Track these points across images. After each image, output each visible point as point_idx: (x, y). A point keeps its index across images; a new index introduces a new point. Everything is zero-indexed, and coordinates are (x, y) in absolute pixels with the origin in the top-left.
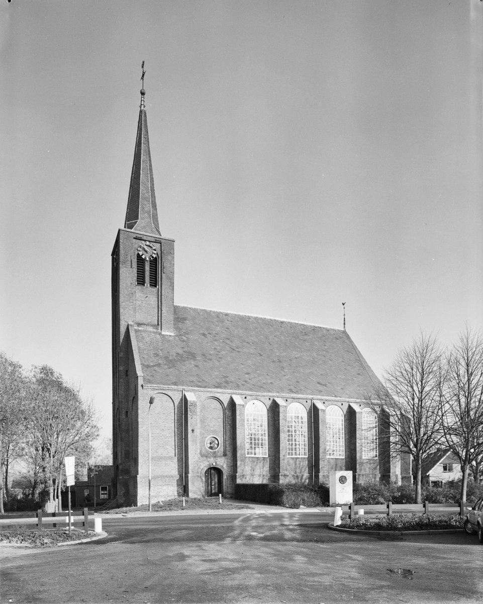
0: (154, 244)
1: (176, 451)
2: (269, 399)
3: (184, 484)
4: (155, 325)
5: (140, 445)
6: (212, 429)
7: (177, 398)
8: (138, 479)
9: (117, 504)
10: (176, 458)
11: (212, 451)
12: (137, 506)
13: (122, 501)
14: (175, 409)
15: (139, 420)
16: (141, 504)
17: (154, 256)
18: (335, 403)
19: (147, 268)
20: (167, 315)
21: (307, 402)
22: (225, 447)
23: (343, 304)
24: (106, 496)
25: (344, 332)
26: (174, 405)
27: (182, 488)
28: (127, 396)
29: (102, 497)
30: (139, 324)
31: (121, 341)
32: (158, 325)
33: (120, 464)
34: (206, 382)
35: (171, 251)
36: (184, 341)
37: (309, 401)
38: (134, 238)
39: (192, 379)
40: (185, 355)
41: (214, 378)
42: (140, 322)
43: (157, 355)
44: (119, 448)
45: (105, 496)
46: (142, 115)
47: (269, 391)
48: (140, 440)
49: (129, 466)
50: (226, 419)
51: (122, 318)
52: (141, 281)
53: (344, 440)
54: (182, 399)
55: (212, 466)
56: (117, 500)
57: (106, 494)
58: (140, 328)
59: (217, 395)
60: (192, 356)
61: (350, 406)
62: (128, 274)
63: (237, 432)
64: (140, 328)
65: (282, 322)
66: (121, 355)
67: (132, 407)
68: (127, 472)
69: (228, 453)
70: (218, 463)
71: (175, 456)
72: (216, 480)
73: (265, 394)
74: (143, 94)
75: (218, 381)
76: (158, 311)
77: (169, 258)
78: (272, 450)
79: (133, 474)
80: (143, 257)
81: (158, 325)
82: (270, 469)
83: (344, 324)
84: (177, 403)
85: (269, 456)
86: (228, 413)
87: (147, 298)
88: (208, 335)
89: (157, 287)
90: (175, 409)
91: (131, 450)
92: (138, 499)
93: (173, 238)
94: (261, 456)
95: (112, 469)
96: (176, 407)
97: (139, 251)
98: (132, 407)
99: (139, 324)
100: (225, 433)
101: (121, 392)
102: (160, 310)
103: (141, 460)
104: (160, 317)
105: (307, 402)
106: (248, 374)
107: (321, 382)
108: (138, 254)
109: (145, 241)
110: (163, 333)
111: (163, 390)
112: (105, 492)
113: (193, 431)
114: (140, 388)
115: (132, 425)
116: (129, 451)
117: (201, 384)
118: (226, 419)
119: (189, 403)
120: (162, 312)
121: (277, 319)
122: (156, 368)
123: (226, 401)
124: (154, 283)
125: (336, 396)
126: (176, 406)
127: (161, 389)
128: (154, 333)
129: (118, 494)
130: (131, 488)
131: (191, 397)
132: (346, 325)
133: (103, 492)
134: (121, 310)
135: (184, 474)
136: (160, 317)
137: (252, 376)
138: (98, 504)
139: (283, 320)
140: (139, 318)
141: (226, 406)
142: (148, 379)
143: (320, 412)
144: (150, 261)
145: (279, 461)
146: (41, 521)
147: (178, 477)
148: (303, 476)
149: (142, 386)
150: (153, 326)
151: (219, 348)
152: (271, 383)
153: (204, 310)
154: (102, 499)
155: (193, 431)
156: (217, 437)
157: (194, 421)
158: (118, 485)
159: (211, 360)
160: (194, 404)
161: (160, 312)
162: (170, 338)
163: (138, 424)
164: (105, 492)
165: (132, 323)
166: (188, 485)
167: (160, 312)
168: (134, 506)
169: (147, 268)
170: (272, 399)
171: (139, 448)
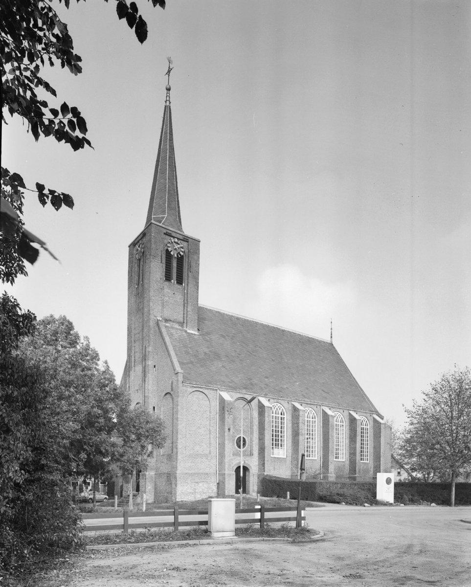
17: (182, 254)
19: (174, 264)
20: (192, 316)
30: (166, 320)
35: (197, 251)
36: (207, 341)
38: (164, 233)
46: (168, 111)
52: (168, 278)
58: (167, 324)
60: (217, 356)
62: (156, 269)
70: (246, 462)
74: (169, 89)
77: (195, 257)
80: (172, 253)
89: (183, 285)
93: (199, 239)
99: (166, 320)
107: (324, 390)
108: (167, 250)
109: (174, 237)
110: (189, 331)
111: (201, 388)
113: (229, 429)
124: (180, 281)
137: (271, 380)
140: (167, 314)
143: (330, 417)
144: (177, 259)
146: (177, 529)
155: (229, 429)
162: (196, 337)
165: (161, 319)
169: (174, 264)
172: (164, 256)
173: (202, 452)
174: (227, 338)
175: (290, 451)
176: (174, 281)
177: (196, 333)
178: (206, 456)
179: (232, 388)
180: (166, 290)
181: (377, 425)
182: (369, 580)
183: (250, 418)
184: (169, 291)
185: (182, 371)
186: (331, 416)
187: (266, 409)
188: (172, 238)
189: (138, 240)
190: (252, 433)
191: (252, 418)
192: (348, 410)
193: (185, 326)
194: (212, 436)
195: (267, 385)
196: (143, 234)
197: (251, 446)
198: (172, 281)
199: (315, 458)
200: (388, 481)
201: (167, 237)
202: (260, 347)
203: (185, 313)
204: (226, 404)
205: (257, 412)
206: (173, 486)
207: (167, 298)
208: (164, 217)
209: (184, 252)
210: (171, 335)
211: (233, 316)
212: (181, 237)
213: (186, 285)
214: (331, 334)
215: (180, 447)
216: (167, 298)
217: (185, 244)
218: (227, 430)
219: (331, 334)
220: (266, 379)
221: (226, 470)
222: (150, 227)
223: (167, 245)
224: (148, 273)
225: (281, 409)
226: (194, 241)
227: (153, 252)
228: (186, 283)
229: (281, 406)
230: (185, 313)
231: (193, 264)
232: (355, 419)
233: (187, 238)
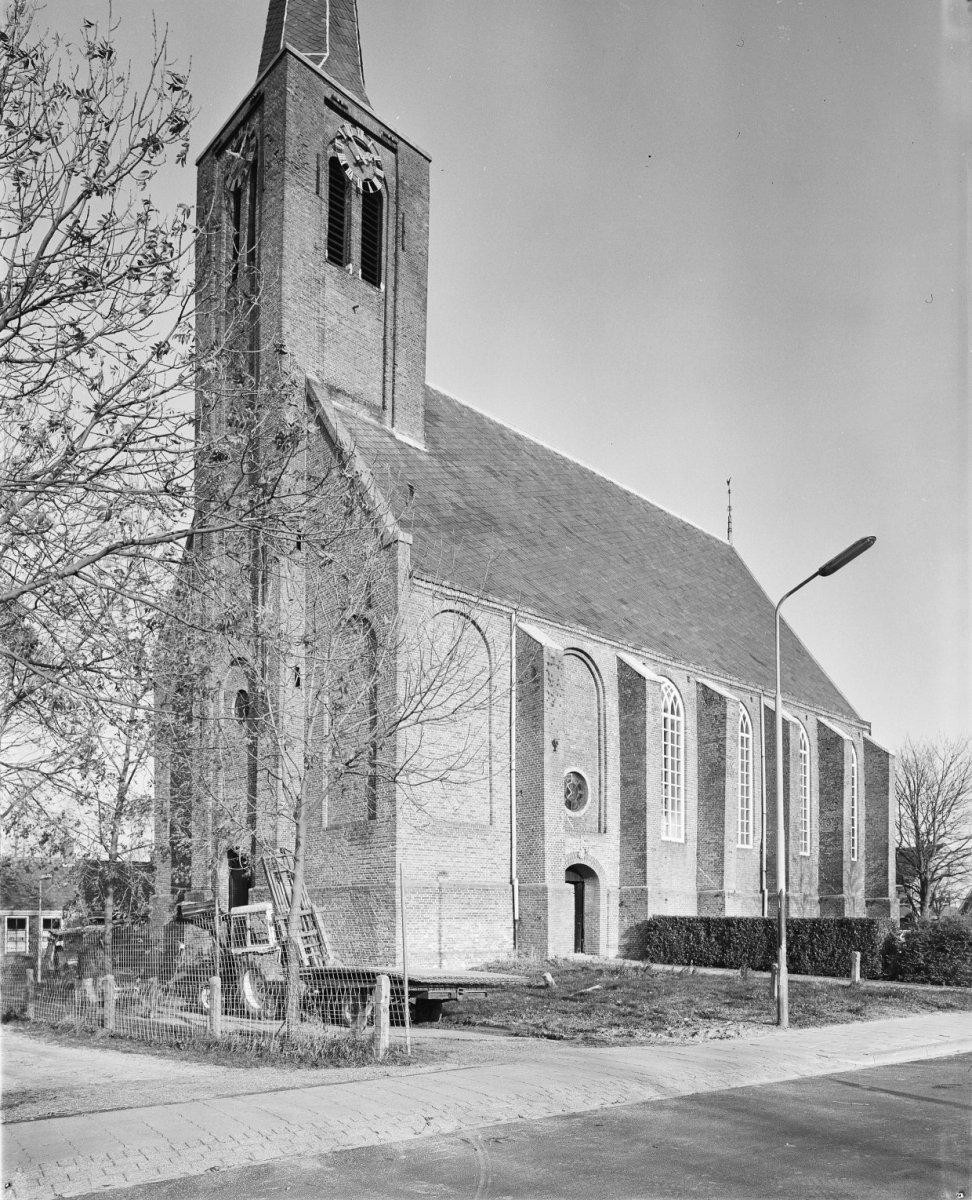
0: (377, 145)
4: (377, 408)
17: (379, 185)
19: (356, 214)
50: (446, 583)
52: (337, 253)
59: (588, 647)
81: (384, 408)
89: (383, 286)
97: (340, 151)
108: (334, 161)
109: (355, 124)
110: (399, 437)
113: (555, 744)
118: (446, 583)
120: (397, 370)
121: (641, 495)
155: (555, 744)
161: (389, 369)
162: (421, 457)
167: (389, 369)
172: (325, 176)
173: (469, 816)
174: (502, 477)
175: (694, 822)
176: (354, 267)
177: (421, 447)
178: (479, 829)
179: (555, 616)
180: (331, 292)
181: (877, 759)
182: (268, 1028)
183: (596, 716)
184: (340, 297)
187: (649, 687)
188: (348, 125)
189: (232, 127)
190: (602, 763)
191: (601, 717)
192: (817, 713)
193: (388, 418)
194: (496, 767)
196: (255, 102)
197: (602, 805)
198: (350, 266)
199: (745, 846)
201: (333, 115)
202: (586, 521)
203: (389, 376)
204: (546, 659)
205: (616, 698)
206: (381, 931)
207: (334, 320)
208: (321, 58)
209: (383, 180)
212: (375, 129)
213: (390, 290)
217: (386, 156)
218: (548, 746)
221: (548, 877)
222: (280, 67)
223: (333, 142)
224: (275, 223)
225: (672, 696)
226: (412, 151)
227: (291, 152)
228: (391, 282)
229: (674, 689)
230: (389, 376)
231: (411, 226)
232: (838, 739)
233: (397, 140)
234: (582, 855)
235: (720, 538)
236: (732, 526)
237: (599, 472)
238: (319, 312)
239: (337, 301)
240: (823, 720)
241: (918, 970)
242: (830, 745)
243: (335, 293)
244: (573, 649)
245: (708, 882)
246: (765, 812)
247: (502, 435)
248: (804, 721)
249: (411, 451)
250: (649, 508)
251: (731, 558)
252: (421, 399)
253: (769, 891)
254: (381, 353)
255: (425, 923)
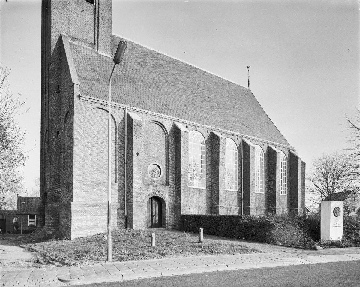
1: (117, 176)
2: (208, 131)
3: (126, 215)
4: (91, 44)
5: (75, 166)
6: (155, 156)
7: (119, 116)
8: (72, 206)
9: (45, 235)
10: (117, 184)
11: (151, 177)
12: (70, 239)
13: (50, 232)
14: (116, 129)
15: (75, 136)
16: (76, 237)
18: (258, 143)
21: (237, 139)
22: (167, 175)
23: (248, 68)
24: (34, 224)
25: (250, 90)
26: (116, 126)
27: (123, 219)
28: (58, 114)
29: (30, 224)
30: (74, 38)
31: (52, 51)
32: (95, 43)
33: (49, 190)
34: (149, 106)
37: (239, 139)
39: (133, 100)
40: (124, 78)
41: (155, 103)
42: (74, 36)
43: (94, 71)
44: (48, 174)
45: (33, 223)
47: (206, 124)
48: (75, 160)
49: (60, 193)
50: (169, 147)
51: (53, 25)
53: (264, 177)
54: (124, 119)
55: (155, 195)
56: (45, 231)
57: (34, 222)
58: (74, 43)
59: (160, 120)
61: (269, 147)
63: (182, 160)
64: (74, 43)
65: (205, 72)
66: (52, 67)
67: (64, 125)
68: (57, 199)
69: (170, 182)
71: (116, 182)
72: (156, 209)
73: (204, 126)
75: (160, 106)
76: (95, 29)
78: (209, 182)
79: (65, 201)
81: (95, 43)
82: (207, 201)
83: (249, 84)
84: (118, 122)
85: (206, 188)
86: (171, 140)
87: (82, 13)
88: (145, 66)
89: (94, 3)
90: (116, 129)
91: (62, 175)
92: (72, 230)
94: (197, 187)
95: (40, 201)
96: (117, 127)
98: (64, 125)
99: (74, 38)
100: (167, 161)
101: (52, 108)
102: (97, 28)
103: (76, 185)
104: (96, 36)
105: (237, 139)
106: (185, 106)
107: (244, 124)
110: (100, 53)
111: (104, 105)
112: (33, 220)
113: (138, 154)
114: (76, 98)
115: (64, 145)
116: (59, 176)
117: (142, 105)
119: (133, 122)
120: (100, 31)
122: (94, 82)
123: (169, 127)
125: (258, 137)
126: (117, 125)
127: (101, 104)
128: (90, 50)
129: (46, 223)
130: (62, 217)
131: (135, 116)
132: (250, 85)
133: (31, 220)
134: (53, 17)
135: (126, 203)
136: (96, 36)
137: (190, 109)
138: (25, 232)
139: (205, 70)
140: (74, 31)
141: (169, 131)
142: (86, 91)
143: (251, 148)
145: (218, 193)
147: (118, 206)
148: (231, 208)
149: (79, 96)
150: (89, 44)
151: (155, 78)
152: (207, 117)
153: (138, 45)
154: (30, 226)
155: (138, 154)
156: (159, 165)
157: (137, 144)
158: (46, 214)
159: (150, 87)
160: (140, 125)
161: (96, 31)
162: (108, 60)
163: (73, 141)
164: (33, 220)
166: (131, 215)
167: (96, 31)
168: (68, 239)
170: (209, 132)
171: (74, 169)
185: (79, 83)
186: (252, 147)
195: (186, 112)
200: (336, 212)
204: (134, 124)
210: (75, 52)
211: (154, 51)
214: (249, 81)
215: (77, 173)
216: (75, 15)
219: (249, 81)
220: (185, 107)
234: (157, 193)
235: (244, 86)
236: (250, 82)
237: (193, 65)
238: (67, 12)
239: (76, 9)
240: (270, 146)
241: (254, 235)
242: (271, 155)
243: (75, 6)
244: (154, 121)
245: (214, 203)
246: (243, 178)
247: (151, 54)
248: (262, 146)
249: (104, 58)
250: (213, 77)
251: (249, 94)
252: (110, 40)
253: (244, 206)
254: (94, 26)
255: (85, 217)
